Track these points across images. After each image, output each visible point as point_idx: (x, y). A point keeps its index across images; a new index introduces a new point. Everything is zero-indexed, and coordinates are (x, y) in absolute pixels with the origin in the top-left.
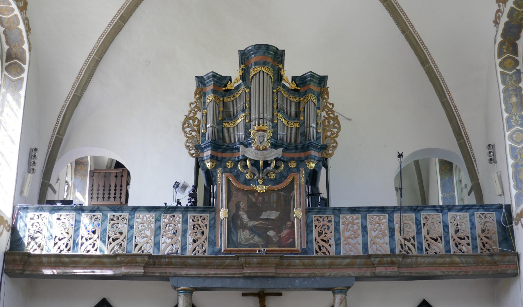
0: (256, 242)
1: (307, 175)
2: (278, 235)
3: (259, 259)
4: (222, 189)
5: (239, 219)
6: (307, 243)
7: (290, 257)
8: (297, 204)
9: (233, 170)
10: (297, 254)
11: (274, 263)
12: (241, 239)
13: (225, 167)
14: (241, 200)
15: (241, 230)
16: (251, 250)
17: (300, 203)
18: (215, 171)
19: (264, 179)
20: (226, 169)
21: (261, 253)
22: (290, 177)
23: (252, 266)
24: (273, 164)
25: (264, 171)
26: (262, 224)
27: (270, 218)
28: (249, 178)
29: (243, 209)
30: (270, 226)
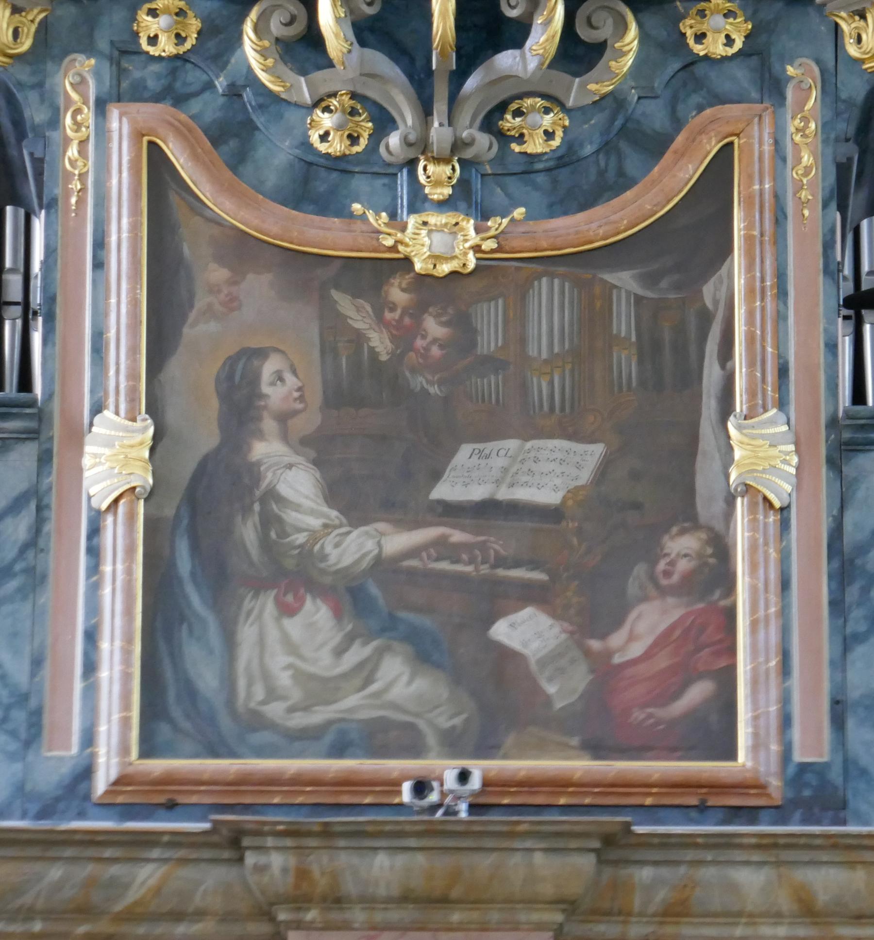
0: (395, 706)
1: (847, 127)
2: (588, 653)
3: (420, 859)
4: (100, 244)
5: (247, 510)
6: (838, 721)
7: (687, 842)
8: (751, 376)
9: (193, 77)
10: (750, 814)
11: (548, 890)
12: (267, 676)
13: (124, 53)
14: (265, 343)
15: (270, 608)
16: (347, 782)
17: (783, 372)
18: (39, 85)
19: (468, 154)
20: (136, 71)
21: (434, 808)
22: (692, 140)
23: (358, 915)
24: (548, 22)
25: (472, 83)
26: (451, 551)
27: (522, 494)
28: (336, 146)
29: (283, 418)
30: (517, 564)
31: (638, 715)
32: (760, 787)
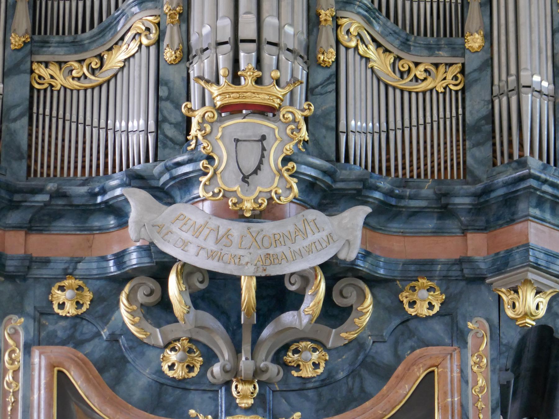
1: (507, 361)
9: (87, 329)
25: (266, 332)
28: (179, 373)
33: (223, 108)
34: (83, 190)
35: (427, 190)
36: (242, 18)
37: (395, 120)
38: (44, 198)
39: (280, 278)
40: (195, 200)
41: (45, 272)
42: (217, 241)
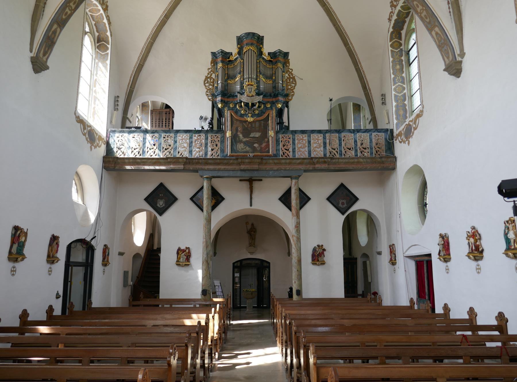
1: (277, 112)
3: (249, 160)
4: (228, 120)
6: (276, 151)
7: (267, 159)
9: (234, 109)
10: (271, 157)
11: (258, 162)
16: (244, 155)
17: (273, 128)
23: (245, 164)
25: (252, 109)
26: (251, 140)
28: (243, 113)
29: (240, 131)
31: (263, 150)
32: (271, 155)
33: (247, 85)
34: (233, 94)
35: (269, 94)
36: (249, 75)
37: (266, 86)
38: (229, 95)
39: (254, 103)
40: (244, 95)
41: (229, 103)
42: (247, 99)
